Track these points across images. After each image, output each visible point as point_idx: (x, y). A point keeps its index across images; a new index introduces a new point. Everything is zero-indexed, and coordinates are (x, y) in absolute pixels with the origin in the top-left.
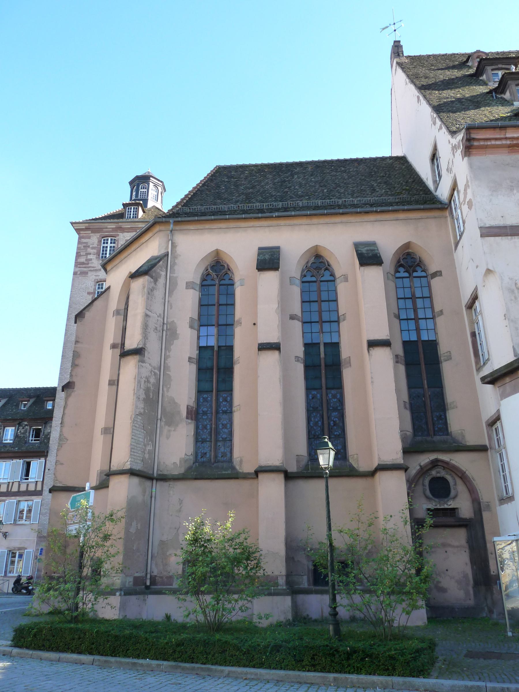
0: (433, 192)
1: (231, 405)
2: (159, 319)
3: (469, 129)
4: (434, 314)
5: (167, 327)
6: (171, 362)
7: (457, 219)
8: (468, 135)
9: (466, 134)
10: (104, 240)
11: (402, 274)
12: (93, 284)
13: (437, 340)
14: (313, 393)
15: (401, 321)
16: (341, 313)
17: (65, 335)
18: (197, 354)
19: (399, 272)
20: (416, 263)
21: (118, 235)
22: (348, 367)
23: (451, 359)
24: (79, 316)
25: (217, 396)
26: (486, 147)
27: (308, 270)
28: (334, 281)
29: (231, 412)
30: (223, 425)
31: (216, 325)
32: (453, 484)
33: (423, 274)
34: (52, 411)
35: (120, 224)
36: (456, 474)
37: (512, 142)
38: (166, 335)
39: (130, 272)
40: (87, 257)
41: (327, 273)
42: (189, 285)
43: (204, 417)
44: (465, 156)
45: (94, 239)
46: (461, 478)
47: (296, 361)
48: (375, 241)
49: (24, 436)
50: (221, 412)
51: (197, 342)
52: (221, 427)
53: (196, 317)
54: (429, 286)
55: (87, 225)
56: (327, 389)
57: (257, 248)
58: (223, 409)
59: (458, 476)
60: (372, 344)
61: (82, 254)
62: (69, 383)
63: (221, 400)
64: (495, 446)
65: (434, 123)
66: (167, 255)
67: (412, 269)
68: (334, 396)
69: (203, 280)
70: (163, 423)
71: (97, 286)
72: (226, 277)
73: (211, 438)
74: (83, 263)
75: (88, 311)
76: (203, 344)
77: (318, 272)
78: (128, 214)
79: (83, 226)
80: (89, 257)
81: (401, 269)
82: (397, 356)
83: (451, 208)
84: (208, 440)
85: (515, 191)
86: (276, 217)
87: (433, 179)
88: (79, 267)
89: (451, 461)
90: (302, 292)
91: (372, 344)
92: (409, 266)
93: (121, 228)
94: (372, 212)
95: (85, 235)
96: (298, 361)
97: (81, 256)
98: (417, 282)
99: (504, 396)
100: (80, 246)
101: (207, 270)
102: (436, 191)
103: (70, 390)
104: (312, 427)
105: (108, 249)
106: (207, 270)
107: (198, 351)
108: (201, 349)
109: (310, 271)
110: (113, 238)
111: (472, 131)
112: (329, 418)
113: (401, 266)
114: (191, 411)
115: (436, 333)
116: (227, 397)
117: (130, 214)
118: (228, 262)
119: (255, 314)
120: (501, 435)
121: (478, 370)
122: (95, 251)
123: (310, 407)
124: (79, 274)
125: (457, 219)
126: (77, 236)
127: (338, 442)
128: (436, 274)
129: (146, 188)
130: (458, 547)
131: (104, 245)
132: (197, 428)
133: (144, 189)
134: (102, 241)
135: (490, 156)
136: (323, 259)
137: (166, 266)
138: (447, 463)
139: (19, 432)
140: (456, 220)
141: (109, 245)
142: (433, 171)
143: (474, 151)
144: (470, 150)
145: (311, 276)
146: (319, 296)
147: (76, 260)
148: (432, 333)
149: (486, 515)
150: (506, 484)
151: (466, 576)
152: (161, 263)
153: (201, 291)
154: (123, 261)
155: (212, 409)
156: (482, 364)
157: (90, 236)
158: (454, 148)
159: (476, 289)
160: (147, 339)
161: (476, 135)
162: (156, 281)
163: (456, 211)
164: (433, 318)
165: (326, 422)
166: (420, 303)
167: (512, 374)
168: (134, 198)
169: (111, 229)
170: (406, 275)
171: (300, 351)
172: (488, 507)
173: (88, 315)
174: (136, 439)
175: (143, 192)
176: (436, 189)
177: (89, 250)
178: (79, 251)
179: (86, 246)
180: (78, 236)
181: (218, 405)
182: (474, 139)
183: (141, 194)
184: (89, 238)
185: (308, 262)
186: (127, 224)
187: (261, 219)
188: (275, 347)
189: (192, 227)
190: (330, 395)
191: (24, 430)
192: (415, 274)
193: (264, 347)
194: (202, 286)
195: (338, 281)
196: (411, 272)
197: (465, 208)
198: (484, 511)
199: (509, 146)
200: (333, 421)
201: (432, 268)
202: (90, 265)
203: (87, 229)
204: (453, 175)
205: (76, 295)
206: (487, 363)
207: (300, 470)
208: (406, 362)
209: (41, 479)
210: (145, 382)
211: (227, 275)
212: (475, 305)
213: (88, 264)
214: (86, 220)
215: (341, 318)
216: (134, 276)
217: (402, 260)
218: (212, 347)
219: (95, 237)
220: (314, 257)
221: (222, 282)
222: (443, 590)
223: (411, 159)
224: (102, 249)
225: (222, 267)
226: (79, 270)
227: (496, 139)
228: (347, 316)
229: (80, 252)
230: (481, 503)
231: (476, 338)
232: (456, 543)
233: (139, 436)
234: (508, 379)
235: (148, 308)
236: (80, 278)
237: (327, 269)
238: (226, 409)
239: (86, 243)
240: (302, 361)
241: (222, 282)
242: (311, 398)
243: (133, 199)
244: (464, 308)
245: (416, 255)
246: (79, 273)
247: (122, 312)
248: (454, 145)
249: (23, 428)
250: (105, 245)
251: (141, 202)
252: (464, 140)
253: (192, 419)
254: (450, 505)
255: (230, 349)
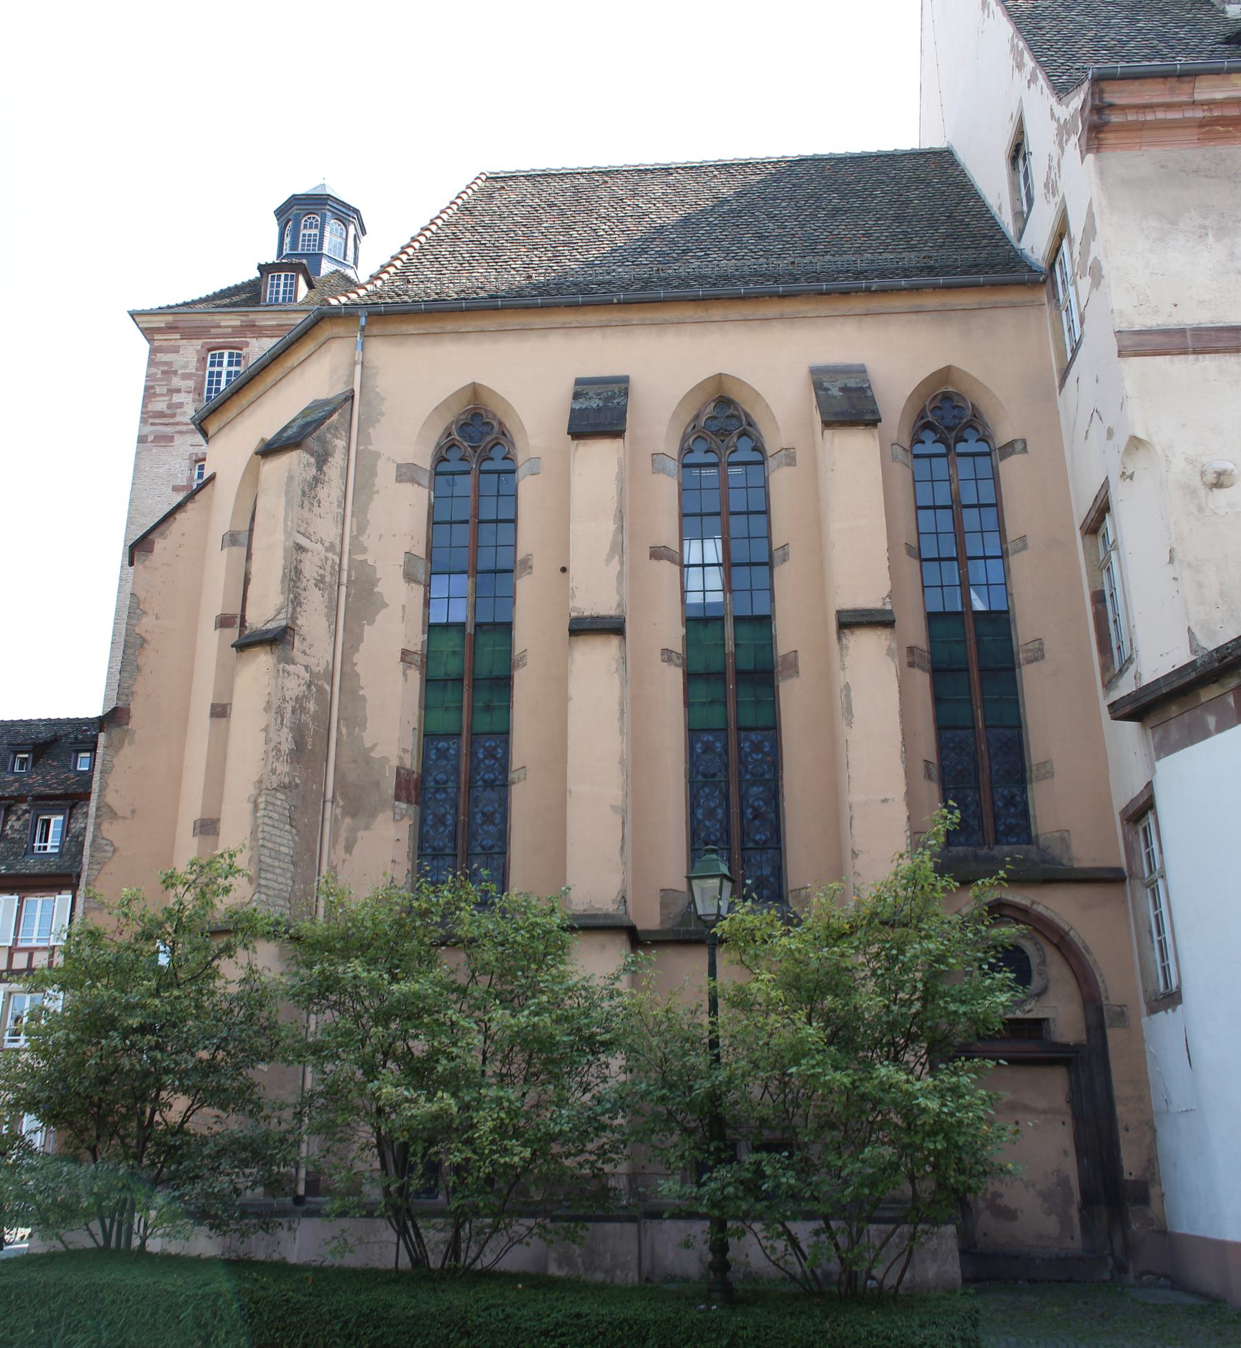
0: (1014, 241)
1: (505, 767)
2: (330, 555)
3: (1098, 80)
4: (1004, 546)
5: (349, 576)
6: (361, 660)
7: (1067, 310)
8: (1097, 96)
9: (1093, 94)
10: (213, 356)
11: (930, 447)
12: (186, 464)
13: (1011, 613)
14: (705, 739)
15: (924, 563)
16: (777, 542)
17: (119, 592)
18: (423, 642)
19: (923, 442)
20: (965, 421)
21: (247, 344)
22: (790, 676)
23: (1043, 657)
24: (139, 548)
25: (472, 743)
26: (1142, 126)
27: (699, 437)
28: (762, 463)
29: (505, 785)
30: (484, 814)
31: (470, 572)
32: (1038, 961)
33: (983, 447)
34: (87, 777)
35: (252, 317)
36: (1047, 938)
37: (1208, 114)
38: (347, 596)
39: (263, 440)
40: (171, 399)
41: (746, 443)
42: (406, 473)
43: (438, 796)
44: (1089, 150)
45: (188, 354)
46: (1057, 946)
47: (663, 661)
48: (863, 366)
49: (20, 838)
50: (480, 783)
51: (424, 614)
52: (479, 821)
53: (421, 551)
54: (996, 478)
55: (170, 318)
56: (740, 729)
57: (572, 382)
58: (486, 777)
59: (1051, 942)
60: (850, 622)
61: (158, 390)
62: (115, 709)
63: (481, 756)
64: (1143, 871)
65: (1020, 66)
66: (350, 397)
67: (954, 434)
68: (757, 748)
69: (440, 459)
70: (339, 811)
71: (197, 471)
72: (497, 453)
73: (455, 848)
74: (161, 415)
75: (162, 535)
76: (438, 617)
77: (723, 441)
78: (271, 293)
79: (160, 322)
80: (177, 398)
81: (928, 436)
82: (911, 650)
83: (1054, 283)
84: (448, 851)
85: (1210, 240)
86: (619, 303)
87: (1013, 209)
88: (152, 424)
89: (1035, 907)
90: (683, 490)
91: (850, 622)
92: (946, 428)
93: (255, 326)
94: (858, 290)
95: (165, 343)
96: (669, 660)
97: (155, 395)
98: (965, 467)
99: (1165, 748)
100: (154, 370)
101: (450, 435)
102: (1019, 240)
103: (116, 732)
104: (699, 822)
105: (224, 378)
106: (450, 435)
107: (426, 636)
108: (432, 629)
109: (703, 438)
110: (235, 351)
111: (1106, 86)
112: (742, 798)
113: (928, 426)
114: (408, 782)
115: (1008, 594)
116: (495, 748)
117: (278, 293)
118: (500, 414)
119: (564, 544)
120: (1155, 845)
121: (1108, 684)
122: (191, 383)
123: (698, 772)
124: (152, 442)
125: (1067, 310)
126: (145, 346)
127: (764, 858)
128: (1009, 449)
129: (316, 227)
130: (1045, 1112)
131: (212, 369)
132: (423, 820)
133: (311, 228)
134: (209, 359)
135: (1152, 149)
136: (736, 408)
137: (346, 426)
138: (1024, 911)
139: (8, 827)
140: (1064, 313)
141: (225, 369)
142: (1015, 188)
143: (1110, 138)
144: (1101, 136)
145: (706, 452)
146: (725, 500)
147: (145, 405)
148: (997, 592)
149: (1114, 1037)
150: (1166, 964)
151: (1063, 1182)
152: (335, 417)
153: (433, 487)
154: (246, 413)
155: (458, 776)
156: (1117, 666)
157: (179, 347)
158: (1063, 130)
159: (1106, 485)
160: (300, 604)
161: (1117, 95)
162: (322, 460)
163: (1065, 290)
164: (1003, 556)
165: (734, 810)
166: (971, 518)
167: (1185, 695)
168: (286, 250)
169: (229, 330)
170: (940, 448)
171: (672, 634)
172: (1121, 1016)
173: (160, 545)
174: (271, 849)
175: (310, 235)
176: (1021, 233)
177: (176, 382)
178: (151, 384)
179: (169, 373)
180: (147, 346)
181: (474, 769)
182: (1111, 106)
183: (304, 241)
184: (176, 350)
185: (697, 417)
186: (229, 317)
187: (582, 309)
188: (612, 627)
189: (411, 328)
190: (748, 744)
191: (20, 823)
192: (961, 448)
193: (583, 628)
194: (437, 474)
195: (771, 463)
196: (952, 442)
197: (1085, 283)
198: (1111, 1026)
199: (1202, 124)
200: (753, 807)
201: (1004, 433)
202: (178, 419)
203: (170, 328)
204: (1058, 199)
205: (144, 494)
206: (1128, 668)
207: (668, 926)
208: (932, 662)
209: (8, 941)
210: (293, 712)
211: (499, 446)
212: (1103, 525)
213: (174, 415)
214: (160, 308)
215: (777, 555)
216: (269, 450)
217: (931, 411)
218: (462, 626)
219: (191, 348)
220: (713, 404)
221: (487, 466)
222: (1009, 1214)
223: (962, 156)
224: (207, 379)
225: (485, 429)
226: (152, 432)
227: (1168, 106)
228: (792, 549)
229: (153, 387)
230: (1105, 1008)
231: (1105, 606)
232: (1041, 1104)
233: (279, 840)
234: (1174, 710)
235: (302, 530)
236: (155, 450)
237: (744, 434)
238: (492, 776)
239: (169, 364)
240: (680, 661)
241: (487, 466)
242: (699, 751)
243: (284, 253)
244: (1078, 533)
245: (964, 400)
246: (150, 438)
247: (244, 538)
248: (1062, 122)
249: (18, 819)
250: (216, 369)
251: (304, 261)
252: (1087, 110)
253: (409, 801)
254: (1030, 1011)
255: (506, 628)
